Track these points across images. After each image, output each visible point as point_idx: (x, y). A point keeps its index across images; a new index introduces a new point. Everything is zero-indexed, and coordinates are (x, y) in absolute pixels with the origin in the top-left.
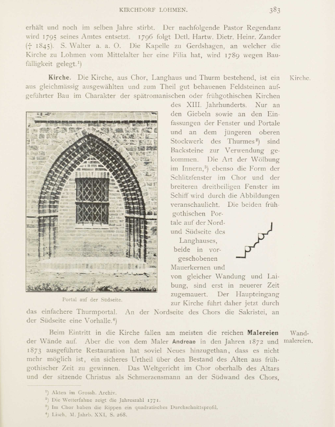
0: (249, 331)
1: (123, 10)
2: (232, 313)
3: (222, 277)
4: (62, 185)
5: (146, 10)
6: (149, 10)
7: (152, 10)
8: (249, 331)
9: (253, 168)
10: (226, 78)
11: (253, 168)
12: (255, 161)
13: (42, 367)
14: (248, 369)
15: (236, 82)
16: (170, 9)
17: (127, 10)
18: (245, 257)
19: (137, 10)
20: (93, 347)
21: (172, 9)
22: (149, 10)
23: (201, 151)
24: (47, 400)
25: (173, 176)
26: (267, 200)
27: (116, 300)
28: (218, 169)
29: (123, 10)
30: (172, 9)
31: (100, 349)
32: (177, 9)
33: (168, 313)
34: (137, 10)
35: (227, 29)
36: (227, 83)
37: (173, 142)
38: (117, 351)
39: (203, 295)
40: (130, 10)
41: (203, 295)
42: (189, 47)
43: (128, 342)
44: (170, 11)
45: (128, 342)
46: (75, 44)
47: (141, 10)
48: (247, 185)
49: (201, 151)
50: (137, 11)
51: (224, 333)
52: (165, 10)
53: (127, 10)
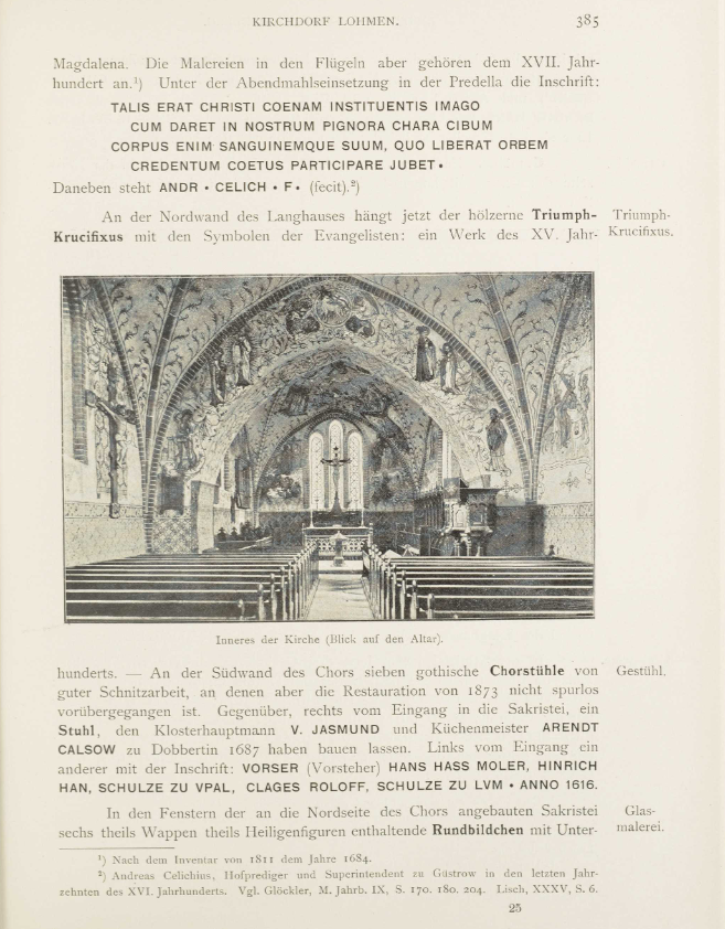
2: (525, 83)
3: (156, 834)
5: (309, 22)
6: (315, 22)
7: (322, 22)
9: (169, 812)
11: (169, 812)
12: (456, 238)
13: (450, 669)
14: (149, 770)
17: (268, 22)
19: (290, 22)
22: (315, 22)
24: (102, 877)
25: (208, 233)
28: (386, 673)
33: (336, 814)
34: (290, 22)
35: (456, 84)
36: (442, 117)
38: (410, 692)
43: (454, 692)
44: (361, 23)
45: (454, 692)
46: (152, 829)
47: (300, 22)
48: (164, 810)
50: (289, 23)
51: (308, 712)
52: (351, 21)
53: (268, 22)
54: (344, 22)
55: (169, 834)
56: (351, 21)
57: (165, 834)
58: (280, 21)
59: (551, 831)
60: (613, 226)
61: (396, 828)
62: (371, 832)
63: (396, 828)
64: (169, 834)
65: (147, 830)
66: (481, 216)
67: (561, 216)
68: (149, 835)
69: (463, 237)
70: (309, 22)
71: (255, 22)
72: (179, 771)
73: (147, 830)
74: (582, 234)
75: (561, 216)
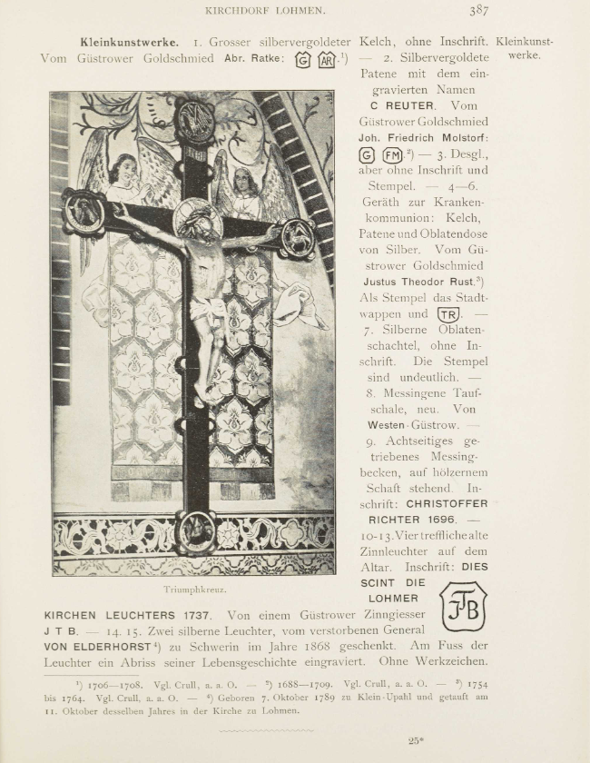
0: (65, 649)
1: (212, 10)
4: (165, 196)
5: (251, 11)
6: (257, 11)
8: (65, 649)
10: (363, 474)
15: (458, 211)
16: (294, 9)
18: (469, 618)
20: (450, 83)
21: (298, 9)
23: (423, 331)
26: (386, 621)
27: (294, 711)
29: (212, 10)
30: (298, 9)
31: (413, 439)
32: (307, 10)
34: (242, 10)
37: (404, 59)
39: (358, 663)
40: (224, 11)
41: (358, 663)
42: (304, 617)
44: (294, 12)
46: (424, 659)
49: (423, 331)
52: (286, 11)
54: (280, 11)
55: (378, 315)
56: (286, 11)
57: (374, 315)
58: (228, 11)
59: (473, 283)
60: (364, 36)
61: (456, 359)
62: (392, 203)
63: (456, 359)
64: (378, 315)
65: (420, 659)
66: (443, 473)
67: (124, 44)
68: (422, 663)
69: (427, 663)
70: (251, 11)
71: (208, 11)
72: (410, 569)
73: (420, 659)
74: (415, 42)
75: (124, 44)
